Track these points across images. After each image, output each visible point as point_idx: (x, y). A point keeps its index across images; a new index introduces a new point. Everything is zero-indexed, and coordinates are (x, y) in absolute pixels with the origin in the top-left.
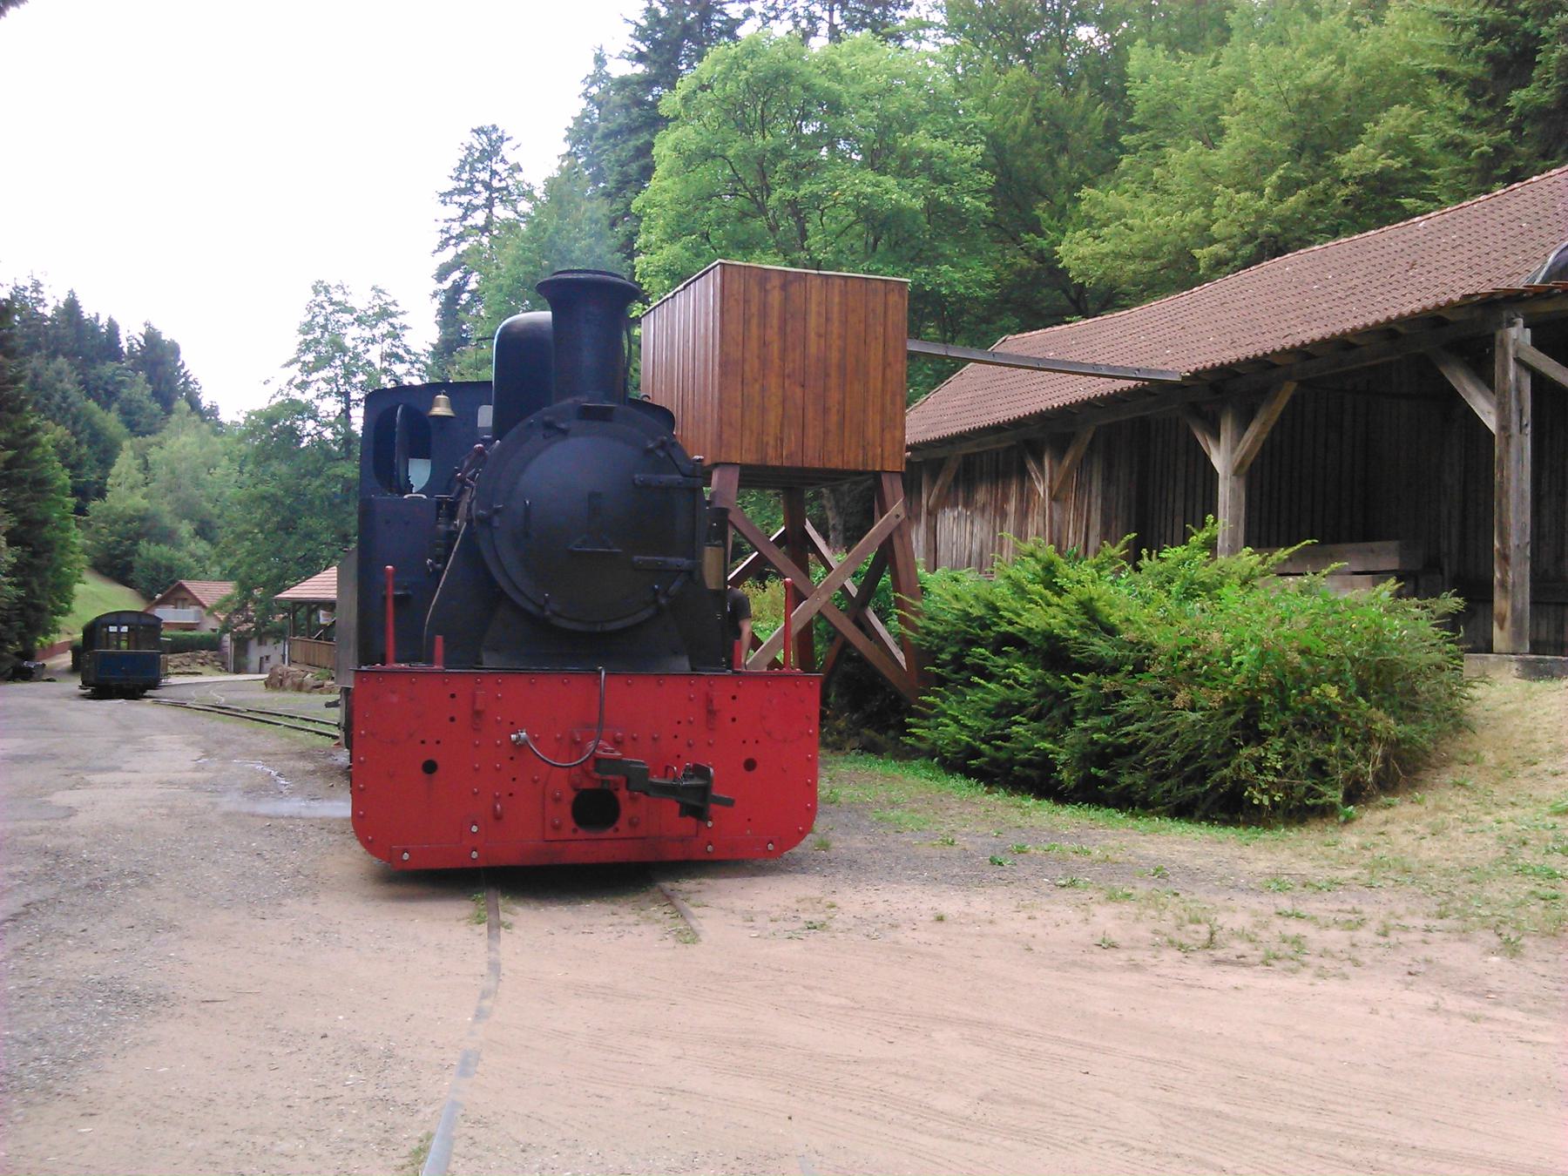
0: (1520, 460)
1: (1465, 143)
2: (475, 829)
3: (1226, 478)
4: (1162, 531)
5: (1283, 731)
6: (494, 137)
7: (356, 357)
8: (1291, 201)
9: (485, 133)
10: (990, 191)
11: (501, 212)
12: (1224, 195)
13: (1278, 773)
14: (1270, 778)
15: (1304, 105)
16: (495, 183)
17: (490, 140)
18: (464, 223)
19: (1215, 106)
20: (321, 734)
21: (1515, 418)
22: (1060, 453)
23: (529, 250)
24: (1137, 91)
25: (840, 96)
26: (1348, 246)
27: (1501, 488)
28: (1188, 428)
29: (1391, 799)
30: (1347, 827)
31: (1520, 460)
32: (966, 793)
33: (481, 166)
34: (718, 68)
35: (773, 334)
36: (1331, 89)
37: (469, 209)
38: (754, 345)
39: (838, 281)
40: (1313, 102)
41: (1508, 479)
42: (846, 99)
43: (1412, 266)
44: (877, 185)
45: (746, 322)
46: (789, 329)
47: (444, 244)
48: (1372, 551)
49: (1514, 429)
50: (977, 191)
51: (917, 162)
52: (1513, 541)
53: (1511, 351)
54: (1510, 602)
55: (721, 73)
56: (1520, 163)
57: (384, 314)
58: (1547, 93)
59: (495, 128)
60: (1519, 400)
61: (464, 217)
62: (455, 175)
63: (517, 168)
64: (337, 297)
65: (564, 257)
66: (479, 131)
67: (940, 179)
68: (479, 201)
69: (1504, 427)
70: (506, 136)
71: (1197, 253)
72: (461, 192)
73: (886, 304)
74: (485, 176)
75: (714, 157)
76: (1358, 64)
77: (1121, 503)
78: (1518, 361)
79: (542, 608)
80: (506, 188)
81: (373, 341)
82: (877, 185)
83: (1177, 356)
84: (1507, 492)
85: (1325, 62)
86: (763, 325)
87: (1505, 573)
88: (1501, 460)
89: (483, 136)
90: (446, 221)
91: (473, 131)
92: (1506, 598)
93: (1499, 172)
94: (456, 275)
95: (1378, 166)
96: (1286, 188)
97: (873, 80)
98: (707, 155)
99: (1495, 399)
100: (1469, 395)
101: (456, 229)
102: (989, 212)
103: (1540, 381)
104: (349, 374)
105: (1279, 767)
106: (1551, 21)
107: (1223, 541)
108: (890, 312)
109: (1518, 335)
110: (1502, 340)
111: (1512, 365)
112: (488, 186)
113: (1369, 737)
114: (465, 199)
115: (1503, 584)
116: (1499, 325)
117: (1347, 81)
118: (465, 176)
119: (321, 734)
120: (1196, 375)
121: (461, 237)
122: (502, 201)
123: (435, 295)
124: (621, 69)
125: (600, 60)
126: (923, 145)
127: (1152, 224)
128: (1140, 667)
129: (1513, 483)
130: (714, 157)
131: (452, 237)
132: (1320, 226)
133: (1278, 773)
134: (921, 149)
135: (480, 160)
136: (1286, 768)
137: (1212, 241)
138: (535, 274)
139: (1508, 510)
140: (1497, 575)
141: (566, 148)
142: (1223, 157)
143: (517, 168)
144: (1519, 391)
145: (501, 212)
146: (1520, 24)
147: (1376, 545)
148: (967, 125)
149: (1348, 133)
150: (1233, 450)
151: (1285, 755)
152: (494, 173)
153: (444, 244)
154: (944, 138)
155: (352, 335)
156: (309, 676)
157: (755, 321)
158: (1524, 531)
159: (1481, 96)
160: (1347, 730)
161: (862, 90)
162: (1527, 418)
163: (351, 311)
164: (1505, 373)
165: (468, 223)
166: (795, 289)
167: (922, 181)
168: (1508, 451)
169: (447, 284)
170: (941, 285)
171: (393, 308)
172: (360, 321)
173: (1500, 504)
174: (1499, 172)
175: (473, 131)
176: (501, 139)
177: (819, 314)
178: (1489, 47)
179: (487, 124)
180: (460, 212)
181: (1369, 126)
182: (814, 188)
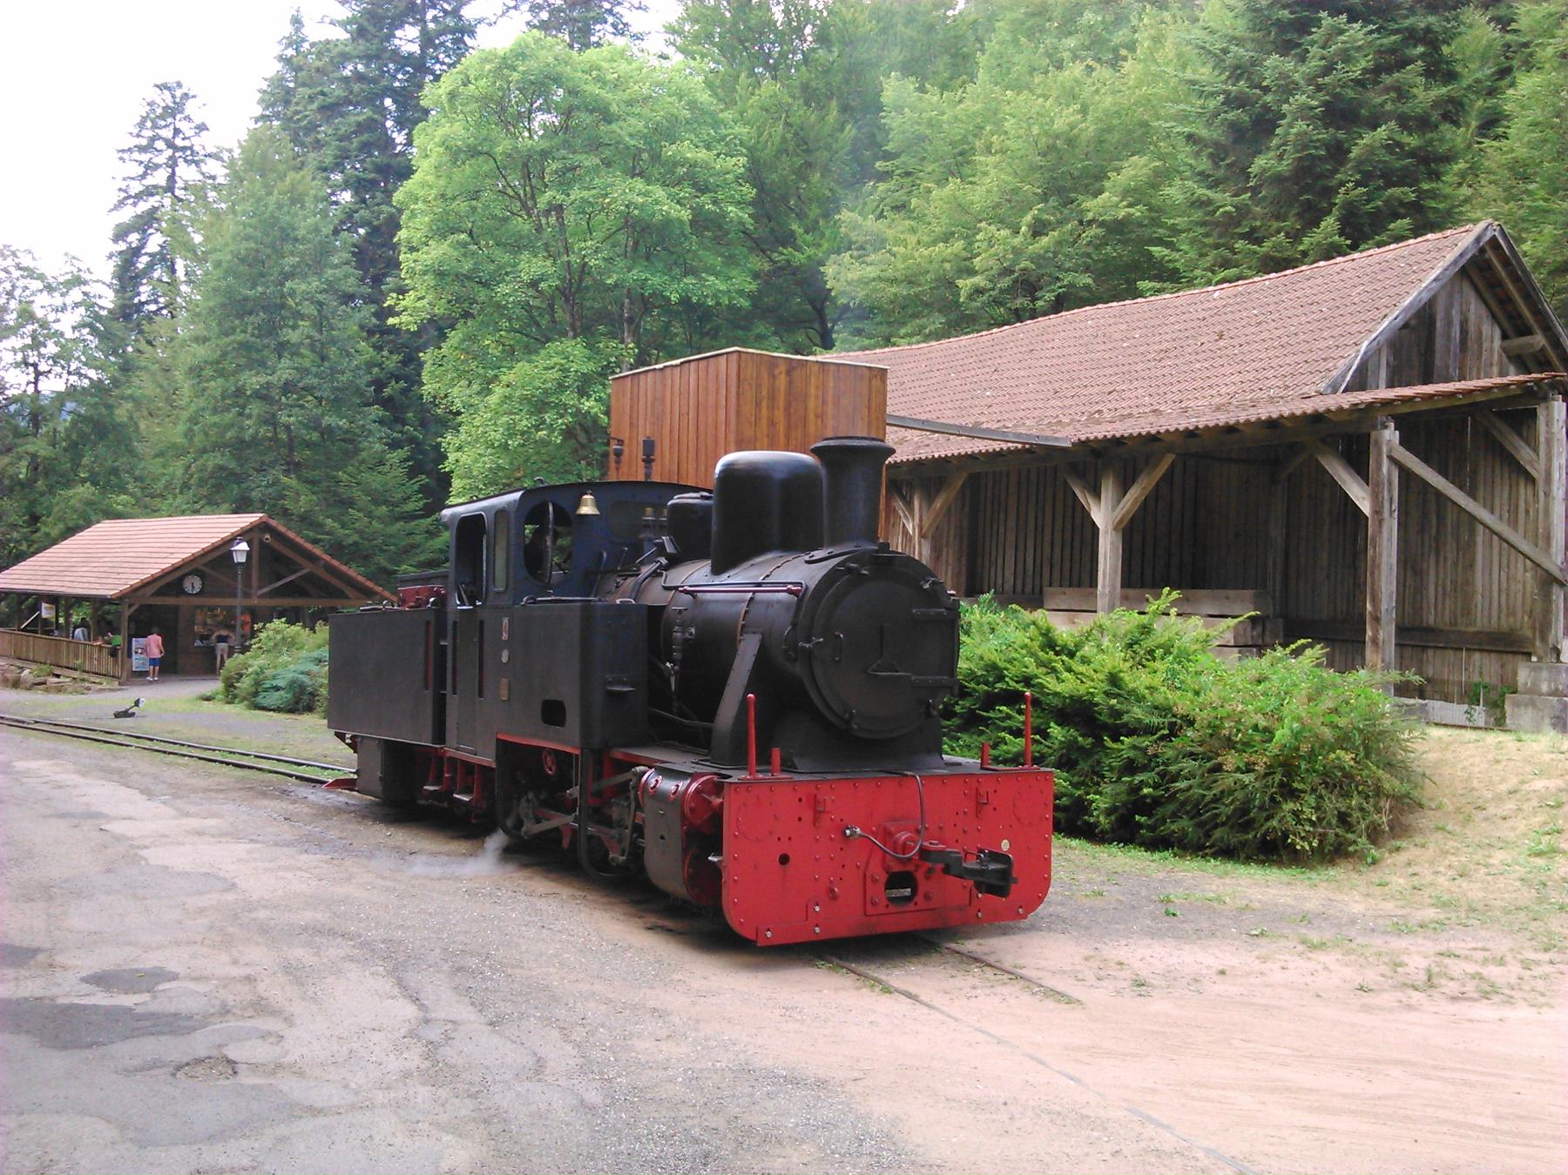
0: (1390, 539)
1: (1209, 202)
2: (817, 909)
3: (1106, 532)
4: (993, 559)
5: (1314, 790)
6: (178, 93)
7: (44, 325)
8: (1045, 241)
9: (168, 89)
10: (750, 204)
11: (186, 173)
12: (988, 230)
13: (1313, 824)
14: (1307, 828)
15: (1051, 148)
16: (179, 142)
17: (173, 97)
18: (144, 182)
19: (964, 140)
20: (228, 764)
21: (1386, 505)
22: (929, 498)
23: (250, 226)
24: (892, 120)
25: (610, 104)
26: (1146, 307)
27: (1374, 561)
28: (1066, 484)
29: (1398, 843)
30: (1372, 868)
31: (1390, 539)
32: (1222, 868)
33: (163, 123)
34: (488, 67)
35: (780, 416)
36: (1077, 137)
37: (150, 168)
38: (764, 423)
39: (832, 368)
40: (1057, 148)
41: (1381, 555)
42: (614, 108)
43: (1221, 336)
44: (647, 194)
45: (758, 404)
46: (792, 411)
47: (121, 204)
48: (1228, 598)
49: (1386, 514)
50: (739, 203)
51: (681, 171)
52: (1384, 606)
53: (1385, 449)
54: (1380, 656)
55: (490, 71)
56: (1258, 223)
57: (77, 281)
58: (1285, 163)
59: (179, 85)
60: (1390, 490)
61: (144, 176)
62: (136, 131)
63: (202, 128)
64: (26, 261)
65: (288, 235)
66: (163, 87)
67: (702, 189)
68: (161, 159)
69: (1377, 512)
70: (191, 94)
71: (960, 283)
72: (142, 149)
73: (870, 388)
74: (167, 133)
75: (480, 153)
76: (1100, 114)
77: (952, 532)
78: (1391, 459)
79: (848, 722)
80: (191, 148)
81: (64, 308)
82: (647, 194)
83: (964, 388)
84: (1379, 565)
85: (1071, 110)
86: (772, 407)
87: (1376, 632)
88: (1374, 539)
89: (166, 92)
90: (124, 179)
91: (157, 86)
92: (1377, 652)
93: (1239, 230)
94: (134, 238)
95: (1122, 214)
96: (1038, 230)
97: (636, 88)
98: (474, 152)
99: (1369, 489)
100: (1344, 483)
101: (136, 187)
102: (749, 223)
103: (1406, 475)
104: (36, 344)
105: (1314, 818)
106: (1291, 100)
107: (1104, 587)
108: (873, 395)
109: (1390, 435)
110: (1376, 441)
111: (1385, 461)
112: (170, 144)
113: (1379, 792)
114: (145, 157)
115: (1375, 641)
116: (1374, 427)
117: (1089, 129)
118: (148, 133)
119: (228, 764)
120: (1083, 444)
121: (139, 197)
122: (186, 161)
123: (110, 256)
124: (316, 32)
125: (297, 22)
126: (689, 155)
127: (916, 254)
128: (1174, 731)
129: (1384, 559)
130: (480, 153)
131: (129, 197)
132: (1067, 265)
133: (1313, 824)
134: (686, 158)
135: (162, 117)
136: (1320, 819)
137: (971, 272)
138: (257, 251)
139: (1379, 581)
140: (1369, 633)
141: (258, 111)
142: (979, 195)
143: (202, 128)
144: (1390, 484)
145: (186, 173)
146: (1259, 97)
147: (1231, 593)
148: (726, 136)
149: (1093, 181)
150: (1114, 509)
151: (1318, 808)
152: (177, 131)
153: (121, 204)
154: (708, 148)
155: (42, 304)
156: (26, 672)
157: (764, 403)
158: (1391, 597)
159: (1223, 160)
160: (1360, 788)
161: (626, 96)
162: (1395, 506)
163: (41, 277)
164: (1379, 468)
165: (146, 182)
166: (797, 374)
167: (686, 192)
168: (1380, 532)
169: (122, 246)
170: (707, 296)
171: (86, 276)
172: (49, 288)
173: (1373, 573)
174: (1239, 230)
175: (157, 86)
176: (186, 96)
177: (817, 397)
178: (1231, 116)
179: (171, 81)
180: (141, 170)
181: (1112, 174)
182: (585, 194)
